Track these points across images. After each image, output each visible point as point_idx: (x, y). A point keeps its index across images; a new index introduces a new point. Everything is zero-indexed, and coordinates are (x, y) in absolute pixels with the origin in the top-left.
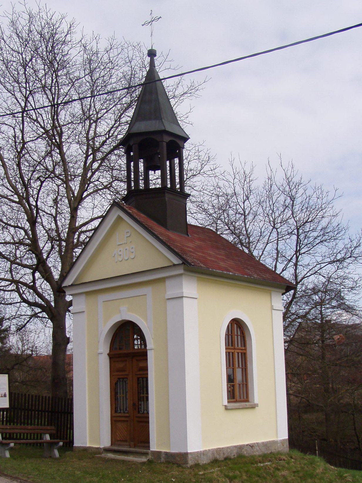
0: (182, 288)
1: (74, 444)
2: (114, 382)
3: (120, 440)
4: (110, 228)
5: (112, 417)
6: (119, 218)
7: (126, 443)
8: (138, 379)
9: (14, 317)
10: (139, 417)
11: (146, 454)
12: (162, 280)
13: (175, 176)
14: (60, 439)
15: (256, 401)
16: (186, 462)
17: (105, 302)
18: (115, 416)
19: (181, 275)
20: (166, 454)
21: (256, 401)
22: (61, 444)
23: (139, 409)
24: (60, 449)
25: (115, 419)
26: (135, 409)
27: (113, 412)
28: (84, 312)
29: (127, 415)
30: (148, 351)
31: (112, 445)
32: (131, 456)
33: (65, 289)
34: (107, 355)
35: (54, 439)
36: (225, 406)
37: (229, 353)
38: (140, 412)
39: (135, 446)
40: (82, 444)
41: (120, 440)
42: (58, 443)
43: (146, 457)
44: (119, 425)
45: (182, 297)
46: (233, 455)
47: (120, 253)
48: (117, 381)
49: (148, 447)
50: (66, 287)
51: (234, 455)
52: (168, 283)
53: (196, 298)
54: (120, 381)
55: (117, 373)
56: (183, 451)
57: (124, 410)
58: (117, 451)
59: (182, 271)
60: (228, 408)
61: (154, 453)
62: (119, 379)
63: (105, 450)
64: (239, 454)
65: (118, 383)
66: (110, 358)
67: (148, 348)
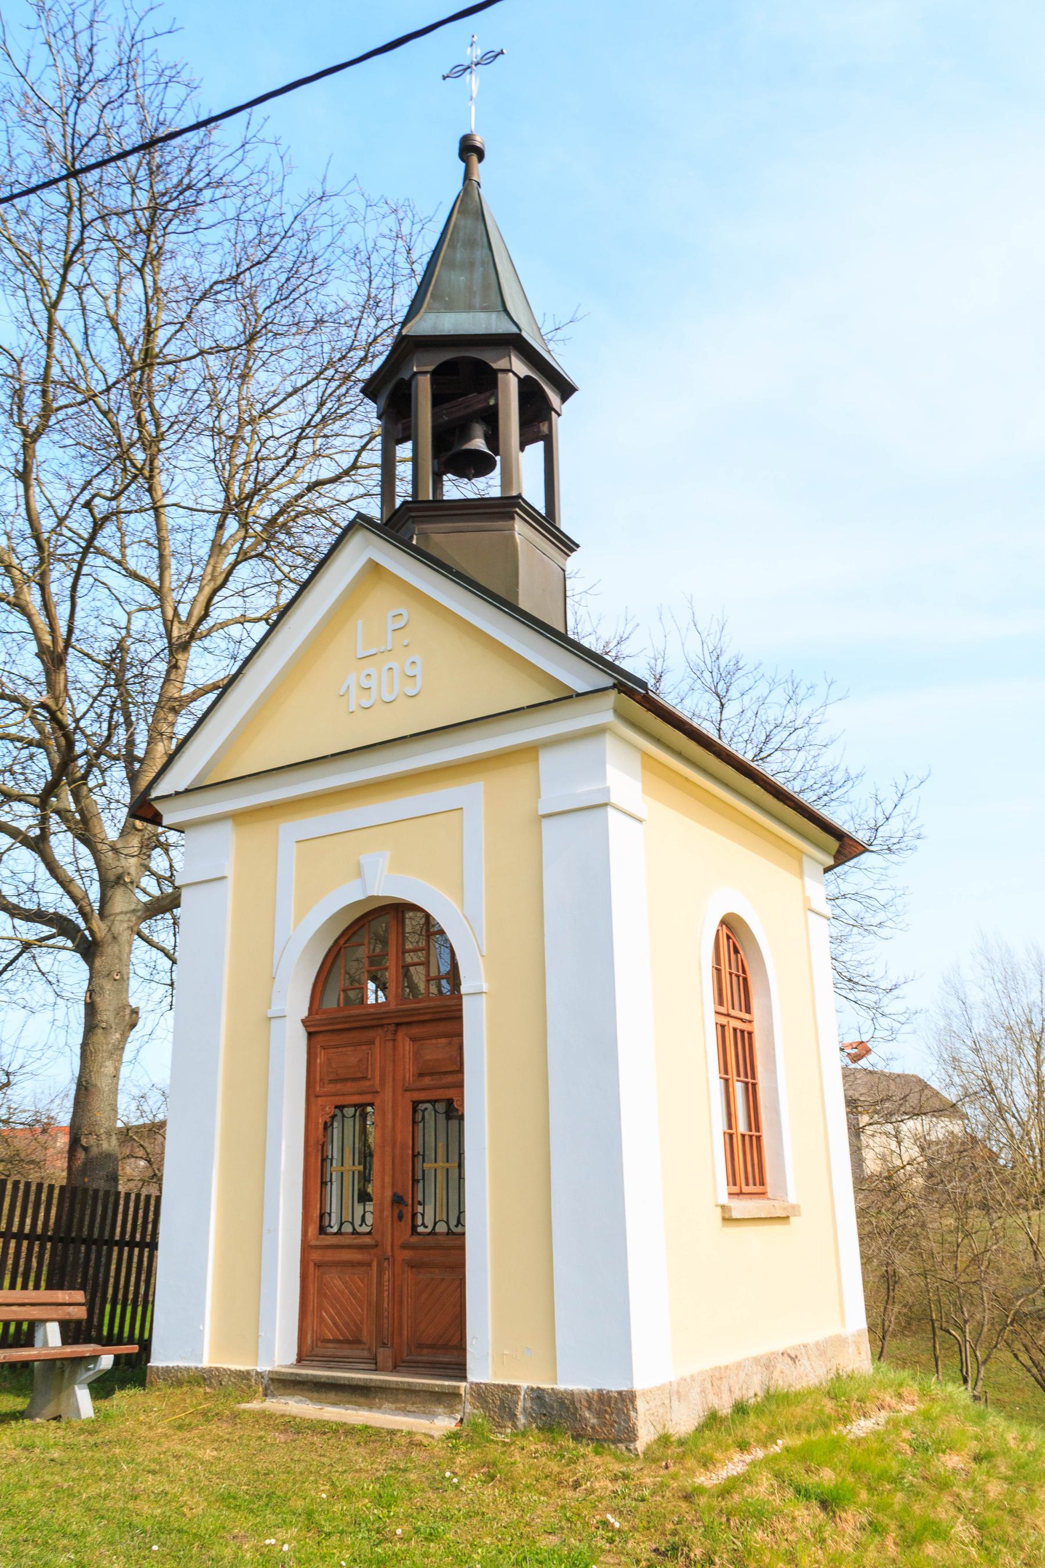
0: (603, 776)
1: (152, 1360)
2: (321, 1121)
3: (336, 1341)
4: (337, 601)
5: (306, 1248)
6: (374, 568)
7: (357, 1353)
8: (415, 1104)
9: (15, 407)
10: (413, 1247)
11: (449, 1399)
12: (530, 751)
13: (7, 1253)
14: (99, 1340)
15: (792, 1198)
16: (630, 1435)
17: (302, 844)
18: (316, 1247)
19: (598, 731)
20: (538, 1397)
21: (792, 1198)
22: (106, 1361)
23: (414, 1216)
24: (101, 1388)
25: (316, 1256)
26: (401, 1217)
27: (313, 1229)
28: (224, 878)
29: (367, 1240)
30: (465, 1000)
31: (300, 1359)
32: (386, 1405)
33: (159, 807)
34: (301, 1024)
35: (76, 1342)
36: (723, 1207)
37: (723, 1027)
38: (421, 1229)
39: (395, 1368)
40: (184, 1359)
41: (336, 1341)
42: (95, 1358)
43: (451, 1411)
44: (335, 1281)
45: (605, 805)
46: (752, 1394)
47: (365, 683)
48: (333, 1117)
49: (459, 1370)
50: (158, 798)
51: (756, 1395)
52: (547, 760)
53: (640, 821)
54: (343, 1116)
55: (329, 1088)
56: (613, 1385)
57: (358, 1221)
58: (291, 1381)
59: (607, 717)
60: (735, 1215)
61: (482, 1394)
62: (340, 1107)
63: (280, 1381)
64: (32, 1390)
65: (335, 1124)
66: (310, 1035)
67: (464, 989)
